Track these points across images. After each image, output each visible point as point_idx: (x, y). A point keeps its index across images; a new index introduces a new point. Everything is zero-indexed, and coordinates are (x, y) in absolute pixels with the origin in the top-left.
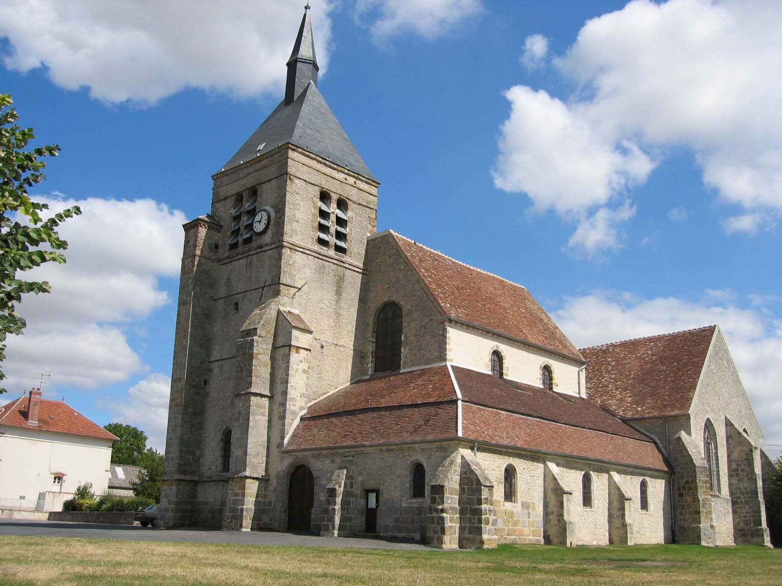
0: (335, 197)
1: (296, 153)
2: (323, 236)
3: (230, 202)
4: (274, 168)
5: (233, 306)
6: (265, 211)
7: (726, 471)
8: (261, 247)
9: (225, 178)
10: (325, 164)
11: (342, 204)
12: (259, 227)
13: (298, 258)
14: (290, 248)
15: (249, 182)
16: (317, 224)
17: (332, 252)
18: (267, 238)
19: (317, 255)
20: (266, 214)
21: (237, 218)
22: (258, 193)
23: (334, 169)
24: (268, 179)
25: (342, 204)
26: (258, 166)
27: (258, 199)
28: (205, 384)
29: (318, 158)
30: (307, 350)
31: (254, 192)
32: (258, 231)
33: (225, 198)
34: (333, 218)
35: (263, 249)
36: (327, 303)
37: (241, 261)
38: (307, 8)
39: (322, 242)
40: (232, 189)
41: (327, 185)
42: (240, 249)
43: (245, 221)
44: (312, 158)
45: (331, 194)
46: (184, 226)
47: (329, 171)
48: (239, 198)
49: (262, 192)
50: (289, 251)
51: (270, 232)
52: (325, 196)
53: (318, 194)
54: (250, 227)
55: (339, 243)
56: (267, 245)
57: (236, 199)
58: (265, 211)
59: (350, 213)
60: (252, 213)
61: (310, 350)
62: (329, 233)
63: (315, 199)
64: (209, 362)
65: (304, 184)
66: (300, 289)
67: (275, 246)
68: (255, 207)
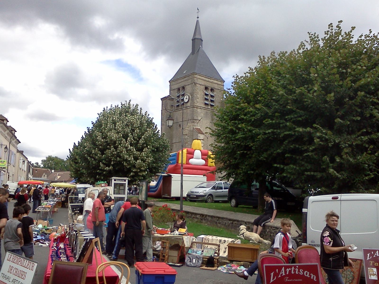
0: (210, 88)
1: (197, 76)
2: (207, 102)
3: (176, 91)
4: (190, 81)
5: (179, 126)
6: (187, 95)
7: (273, 216)
8: (187, 107)
9: (174, 82)
10: (206, 77)
11: (212, 90)
12: (186, 101)
13: (199, 110)
14: (196, 108)
15: (182, 84)
16: (204, 98)
17: (209, 107)
18: (189, 104)
19: (205, 109)
20: (188, 96)
21: (178, 97)
22: (185, 88)
23: (209, 79)
24: (188, 84)
25: (212, 90)
26: (184, 79)
27: (185, 90)
28: (171, 150)
29: (204, 76)
30: (202, 140)
31: (183, 88)
32: (186, 102)
33: (174, 90)
34: (210, 95)
35: (188, 108)
36: (208, 124)
37: (181, 111)
38: (198, 18)
39: (206, 104)
40: (176, 87)
41: (208, 84)
42: (180, 107)
43: (181, 98)
44: (202, 76)
45: (209, 87)
46: (161, 99)
47: (207, 79)
48: (179, 89)
49: (186, 88)
50: (196, 109)
51: (190, 102)
52: (206, 88)
53: (204, 88)
54: (183, 100)
55: (212, 99)
56: (189, 107)
57: (178, 90)
58: (187, 95)
59: (215, 93)
60: (183, 95)
61: (204, 140)
62: (208, 101)
63: (203, 90)
64: (172, 143)
65: (199, 85)
66: (200, 120)
67: (191, 107)
68: (184, 94)
